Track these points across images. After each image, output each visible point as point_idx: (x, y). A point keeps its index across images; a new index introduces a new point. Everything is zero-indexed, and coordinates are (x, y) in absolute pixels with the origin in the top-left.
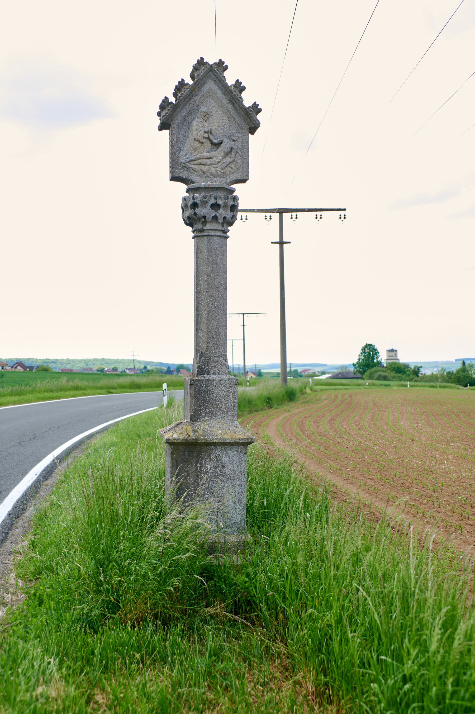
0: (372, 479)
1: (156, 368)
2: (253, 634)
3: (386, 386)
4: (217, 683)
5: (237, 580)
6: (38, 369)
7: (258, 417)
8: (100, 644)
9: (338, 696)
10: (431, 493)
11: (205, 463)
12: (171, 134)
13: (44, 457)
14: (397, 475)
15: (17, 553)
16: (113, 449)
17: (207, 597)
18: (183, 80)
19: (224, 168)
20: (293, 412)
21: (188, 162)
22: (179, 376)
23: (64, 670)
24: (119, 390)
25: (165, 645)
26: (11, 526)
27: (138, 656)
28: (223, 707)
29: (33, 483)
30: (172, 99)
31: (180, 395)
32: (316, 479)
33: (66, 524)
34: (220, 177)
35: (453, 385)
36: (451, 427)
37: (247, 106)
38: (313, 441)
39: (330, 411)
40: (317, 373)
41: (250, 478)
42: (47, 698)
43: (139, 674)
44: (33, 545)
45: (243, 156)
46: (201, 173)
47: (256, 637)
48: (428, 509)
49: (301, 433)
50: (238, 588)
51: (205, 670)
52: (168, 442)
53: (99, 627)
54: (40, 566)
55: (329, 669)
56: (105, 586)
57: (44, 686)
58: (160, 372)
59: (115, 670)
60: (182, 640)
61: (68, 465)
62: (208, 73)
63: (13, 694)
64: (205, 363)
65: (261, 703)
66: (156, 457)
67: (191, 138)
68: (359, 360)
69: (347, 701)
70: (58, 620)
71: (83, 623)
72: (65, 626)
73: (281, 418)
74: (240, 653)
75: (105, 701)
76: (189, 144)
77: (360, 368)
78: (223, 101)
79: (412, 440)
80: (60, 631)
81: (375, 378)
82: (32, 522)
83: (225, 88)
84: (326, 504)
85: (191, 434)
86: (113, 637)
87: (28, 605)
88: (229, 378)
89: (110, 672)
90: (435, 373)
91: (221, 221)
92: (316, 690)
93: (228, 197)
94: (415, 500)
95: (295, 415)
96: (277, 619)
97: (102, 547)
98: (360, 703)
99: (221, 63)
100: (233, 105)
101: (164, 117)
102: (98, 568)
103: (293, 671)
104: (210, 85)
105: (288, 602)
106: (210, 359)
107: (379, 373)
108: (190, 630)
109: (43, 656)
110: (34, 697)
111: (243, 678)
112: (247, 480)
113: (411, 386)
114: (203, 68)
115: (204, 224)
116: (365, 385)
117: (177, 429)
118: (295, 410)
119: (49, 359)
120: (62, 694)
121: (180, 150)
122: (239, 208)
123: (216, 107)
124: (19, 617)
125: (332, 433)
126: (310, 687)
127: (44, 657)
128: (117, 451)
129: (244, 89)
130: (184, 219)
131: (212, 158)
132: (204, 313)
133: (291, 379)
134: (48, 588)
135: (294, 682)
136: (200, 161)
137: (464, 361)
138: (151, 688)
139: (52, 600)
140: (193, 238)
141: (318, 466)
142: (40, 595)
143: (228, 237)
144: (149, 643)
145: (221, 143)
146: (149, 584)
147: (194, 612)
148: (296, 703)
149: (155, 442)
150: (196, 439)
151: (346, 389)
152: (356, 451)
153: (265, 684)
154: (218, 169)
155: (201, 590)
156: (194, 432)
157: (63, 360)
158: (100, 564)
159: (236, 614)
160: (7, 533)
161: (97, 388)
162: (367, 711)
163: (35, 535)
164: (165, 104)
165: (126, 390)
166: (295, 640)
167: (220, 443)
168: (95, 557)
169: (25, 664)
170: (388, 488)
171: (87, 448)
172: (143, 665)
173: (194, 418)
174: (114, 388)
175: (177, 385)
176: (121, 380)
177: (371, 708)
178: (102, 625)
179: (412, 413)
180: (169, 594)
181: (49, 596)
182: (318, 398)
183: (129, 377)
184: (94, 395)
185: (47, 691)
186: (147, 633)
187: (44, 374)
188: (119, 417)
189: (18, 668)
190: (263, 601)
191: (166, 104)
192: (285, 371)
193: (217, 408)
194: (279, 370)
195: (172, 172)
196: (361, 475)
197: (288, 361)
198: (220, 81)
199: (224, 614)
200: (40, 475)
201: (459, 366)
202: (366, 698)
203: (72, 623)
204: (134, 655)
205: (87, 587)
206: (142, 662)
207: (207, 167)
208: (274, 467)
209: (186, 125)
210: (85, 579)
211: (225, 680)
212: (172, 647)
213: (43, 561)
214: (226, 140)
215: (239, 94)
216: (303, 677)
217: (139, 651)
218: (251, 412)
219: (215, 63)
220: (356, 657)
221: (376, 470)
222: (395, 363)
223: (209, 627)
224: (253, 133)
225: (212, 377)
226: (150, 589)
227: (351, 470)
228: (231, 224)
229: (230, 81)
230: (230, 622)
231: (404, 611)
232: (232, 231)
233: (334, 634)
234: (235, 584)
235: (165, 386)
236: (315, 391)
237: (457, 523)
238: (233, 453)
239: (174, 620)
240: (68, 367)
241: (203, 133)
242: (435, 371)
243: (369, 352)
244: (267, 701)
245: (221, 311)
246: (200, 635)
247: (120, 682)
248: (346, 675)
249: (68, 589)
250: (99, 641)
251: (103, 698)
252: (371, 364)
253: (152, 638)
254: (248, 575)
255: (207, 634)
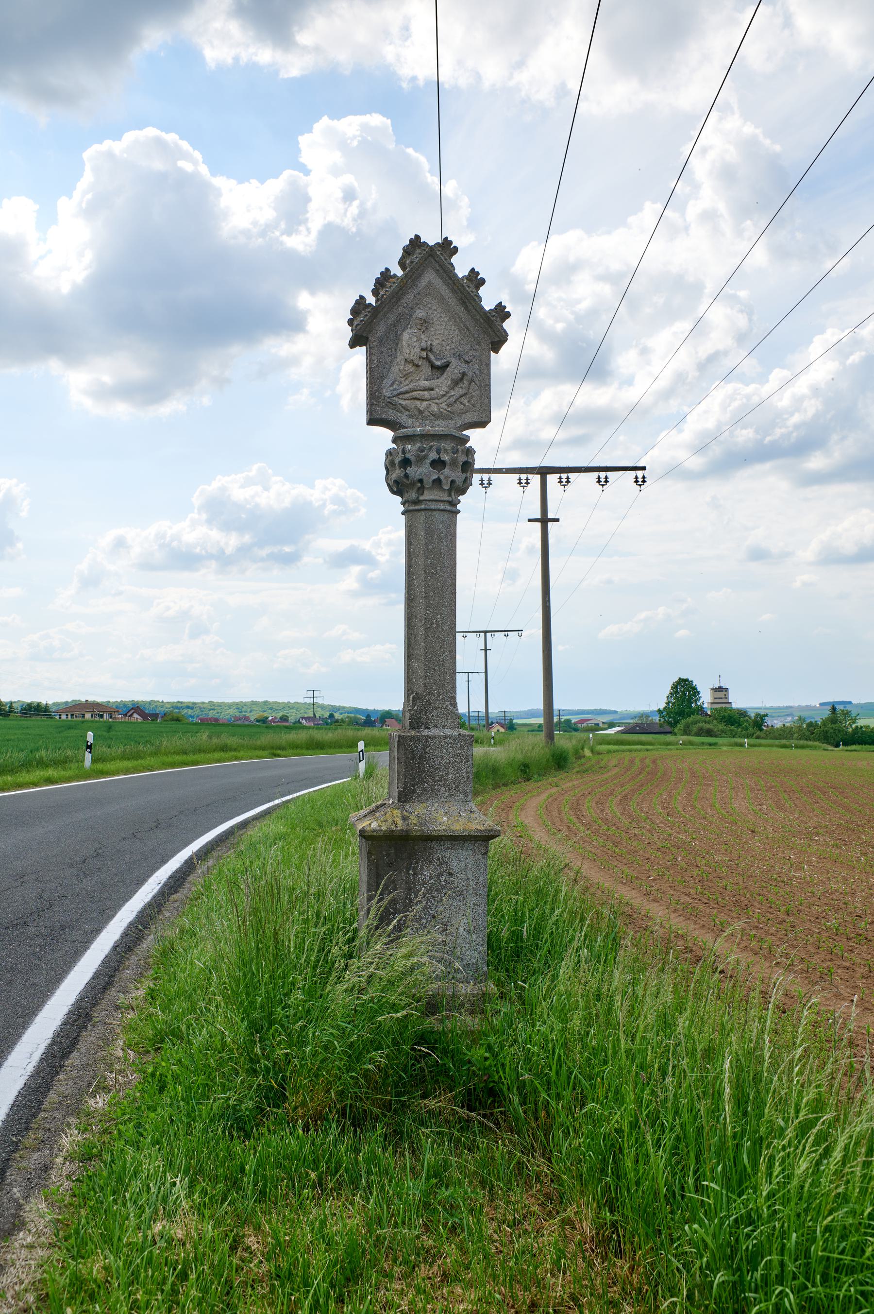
0: (688, 894)
1: (348, 717)
2: (497, 1143)
3: (710, 745)
4: (439, 1221)
5: (472, 1056)
6: (166, 718)
7: (508, 794)
8: (255, 1155)
9: (632, 1243)
10: (782, 915)
11: (422, 869)
12: (370, 355)
13: (172, 856)
14: (728, 888)
15: (127, 1009)
16: (280, 844)
17: (425, 1080)
18: (387, 270)
19: (452, 405)
20: (564, 787)
21: (396, 396)
22: (384, 730)
23: (196, 1195)
24: (289, 752)
25: (356, 1159)
26: (118, 966)
27: (313, 1175)
28: (448, 1261)
29: (154, 897)
30: (371, 300)
31: (383, 757)
32: (599, 893)
33: (204, 964)
34: (446, 418)
35: (817, 743)
36: (814, 810)
37: (487, 308)
38: (595, 832)
39: (622, 786)
40: (601, 725)
41: (492, 893)
42: (170, 1241)
43: (315, 1205)
44: (152, 995)
45: (481, 385)
46: (416, 413)
47: (501, 1148)
48: (778, 943)
49: (575, 820)
50: (474, 1068)
51: (420, 1200)
52: (363, 834)
53: (252, 1128)
54: (162, 1029)
55: (617, 1201)
56: (264, 1063)
57: (164, 1222)
58: (354, 723)
59: (276, 1198)
60: (383, 1151)
61: (208, 868)
62: (428, 258)
63: (117, 1233)
64: (422, 711)
65: (508, 1254)
66: (346, 857)
67: (400, 358)
68: (668, 703)
69: (647, 1252)
70: (188, 1115)
71: (227, 1121)
72: (199, 1126)
73: (545, 796)
74: (475, 1172)
75: (261, 1248)
76: (398, 366)
77: (670, 717)
78: (450, 300)
79: (753, 832)
80: (191, 1134)
81: (693, 733)
82: (151, 960)
83: (453, 281)
84: (613, 934)
85: (399, 822)
86: (274, 1144)
87: (143, 1091)
88: (460, 735)
89: (270, 1200)
90: (788, 725)
91: (446, 488)
92: (598, 1234)
93: (458, 450)
94: (756, 927)
95: (566, 792)
96: (537, 1119)
97: (259, 1000)
98: (666, 1256)
99: (416, 236)
100: (466, 308)
101: (358, 327)
102: (252, 1034)
103: (561, 1203)
104: (430, 277)
105: (553, 1092)
106: (430, 704)
107: (700, 725)
108: (396, 1136)
109: (164, 1172)
110: (149, 1238)
111: (481, 1213)
112: (488, 896)
113: (750, 745)
114: (418, 251)
115: (420, 492)
116: (677, 744)
117: (377, 814)
118: (568, 783)
119: (181, 703)
120: (195, 1235)
121: (382, 377)
122: (476, 466)
123: (439, 310)
124: (128, 1110)
125: (626, 821)
126: (587, 1227)
127: (165, 1174)
128: (286, 848)
129: (482, 282)
130: (388, 485)
131: (432, 389)
132: (421, 632)
133: (559, 734)
134: (174, 1064)
135: (563, 1221)
136: (413, 393)
137: (833, 706)
138: (333, 1228)
139: (180, 1084)
140: (403, 513)
141: (602, 873)
142: (161, 1075)
143: (459, 511)
144: (331, 1154)
145: (448, 366)
146: (335, 1061)
147: (402, 1106)
148: (565, 1255)
149: (345, 833)
150: (407, 831)
151: (647, 750)
152: (663, 850)
153: (515, 1224)
154: (443, 405)
155: (414, 1070)
156: (404, 819)
157: (203, 703)
158: (255, 1027)
159: (471, 1109)
160: (112, 976)
161: (256, 749)
162: (678, 1269)
163: (155, 979)
164: (360, 306)
165: (301, 752)
166: (564, 1153)
167: (445, 836)
168: (248, 1016)
169: (136, 1185)
170: (713, 908)
171: (238, 843)
172: (322, 1190)
173: (404, 797)
174: (283, 748)
175: (380, 744)
176: (292, 736)
177: (684, 1265)
178: (257, 1125)
179: (752, 789)
180: (366, 1075)
181: (176, 1078)
182: (602, 764)
183: (305, 731)
184: (251, 758)
185: (170, 1230)
186: (328, 1139)
187: (174, 725)
188: (289, 794)
189: (125, 1192)
190: (515, 1089)
191: (361, 307)
192: (552, 723)
193: (441, 781)
194: (541, 720)
195: (371, 411)
196: (671, 887)
197: (556, 706)
198: (445, 272)
199: (452, 1109)
200: (165, 884)
201: (826, 713)
202: (677, 1248)
203: (211, 1121)
204: (307, 1174)
205: (236, 1064)
206: (321, 1185)
207: (425, 403)
208: (531, 875)
209: (393, 338)
210: (231, 1050)
211: (452, 1216)
212: (368, 1161)
213: (166, 1022)
214: (453, 360)
215: (474, 290)
216: (576, 1213)
217: (315, 1166)
218: (496, 787)
219: (438, 244)
220: (662, 1182)
221: (694, 879)
222: (725, 709)
223: (427, 1131)
224: (496, 351)
225: (432, 732)
226: (336, 1068)
227: (656, 880)
228: (463, 492)
229: (461, 272)
230: (460, 1123)
231: (739, 1108)
232: (465, 502)
233: (626, 1145)
234: (469, 1062)
235: (361, 745)
236: (599, 754)
237: (824, 965)
238: (465, 853)
239: (371, 1119)
240: (211, 714)
241: (419, 350)
242: (788, 721)
243: (684, 690)
244: (518, 1251)
245: (446, 628)
246: (413, 1143)
247: (284, 1216)
248: (645, 1211)
249: (204, 1066)
250: (252, 1152)
251: (258, 1243)
252: (687, 710)
253: (336, 1147)
254: (489, 1048)
255: (423, 1141)
